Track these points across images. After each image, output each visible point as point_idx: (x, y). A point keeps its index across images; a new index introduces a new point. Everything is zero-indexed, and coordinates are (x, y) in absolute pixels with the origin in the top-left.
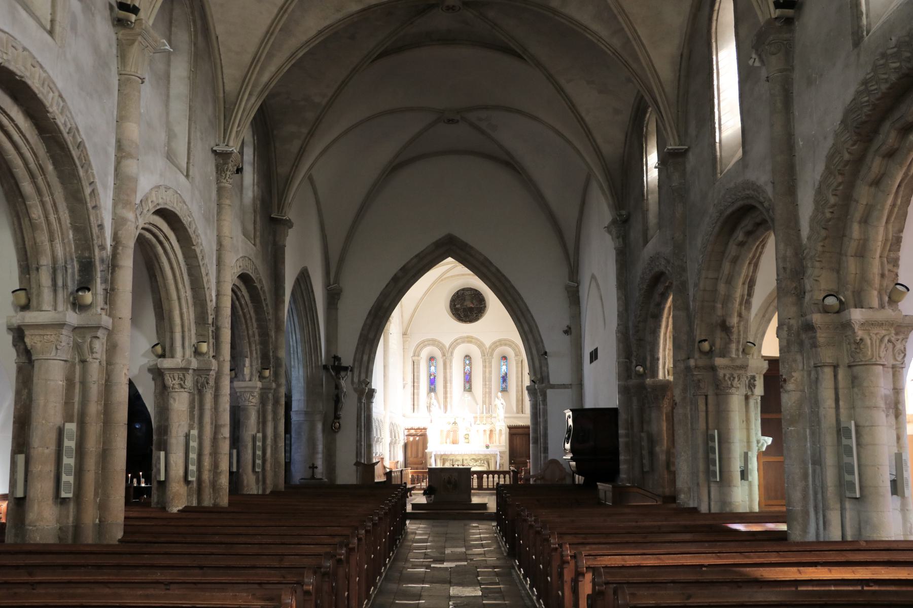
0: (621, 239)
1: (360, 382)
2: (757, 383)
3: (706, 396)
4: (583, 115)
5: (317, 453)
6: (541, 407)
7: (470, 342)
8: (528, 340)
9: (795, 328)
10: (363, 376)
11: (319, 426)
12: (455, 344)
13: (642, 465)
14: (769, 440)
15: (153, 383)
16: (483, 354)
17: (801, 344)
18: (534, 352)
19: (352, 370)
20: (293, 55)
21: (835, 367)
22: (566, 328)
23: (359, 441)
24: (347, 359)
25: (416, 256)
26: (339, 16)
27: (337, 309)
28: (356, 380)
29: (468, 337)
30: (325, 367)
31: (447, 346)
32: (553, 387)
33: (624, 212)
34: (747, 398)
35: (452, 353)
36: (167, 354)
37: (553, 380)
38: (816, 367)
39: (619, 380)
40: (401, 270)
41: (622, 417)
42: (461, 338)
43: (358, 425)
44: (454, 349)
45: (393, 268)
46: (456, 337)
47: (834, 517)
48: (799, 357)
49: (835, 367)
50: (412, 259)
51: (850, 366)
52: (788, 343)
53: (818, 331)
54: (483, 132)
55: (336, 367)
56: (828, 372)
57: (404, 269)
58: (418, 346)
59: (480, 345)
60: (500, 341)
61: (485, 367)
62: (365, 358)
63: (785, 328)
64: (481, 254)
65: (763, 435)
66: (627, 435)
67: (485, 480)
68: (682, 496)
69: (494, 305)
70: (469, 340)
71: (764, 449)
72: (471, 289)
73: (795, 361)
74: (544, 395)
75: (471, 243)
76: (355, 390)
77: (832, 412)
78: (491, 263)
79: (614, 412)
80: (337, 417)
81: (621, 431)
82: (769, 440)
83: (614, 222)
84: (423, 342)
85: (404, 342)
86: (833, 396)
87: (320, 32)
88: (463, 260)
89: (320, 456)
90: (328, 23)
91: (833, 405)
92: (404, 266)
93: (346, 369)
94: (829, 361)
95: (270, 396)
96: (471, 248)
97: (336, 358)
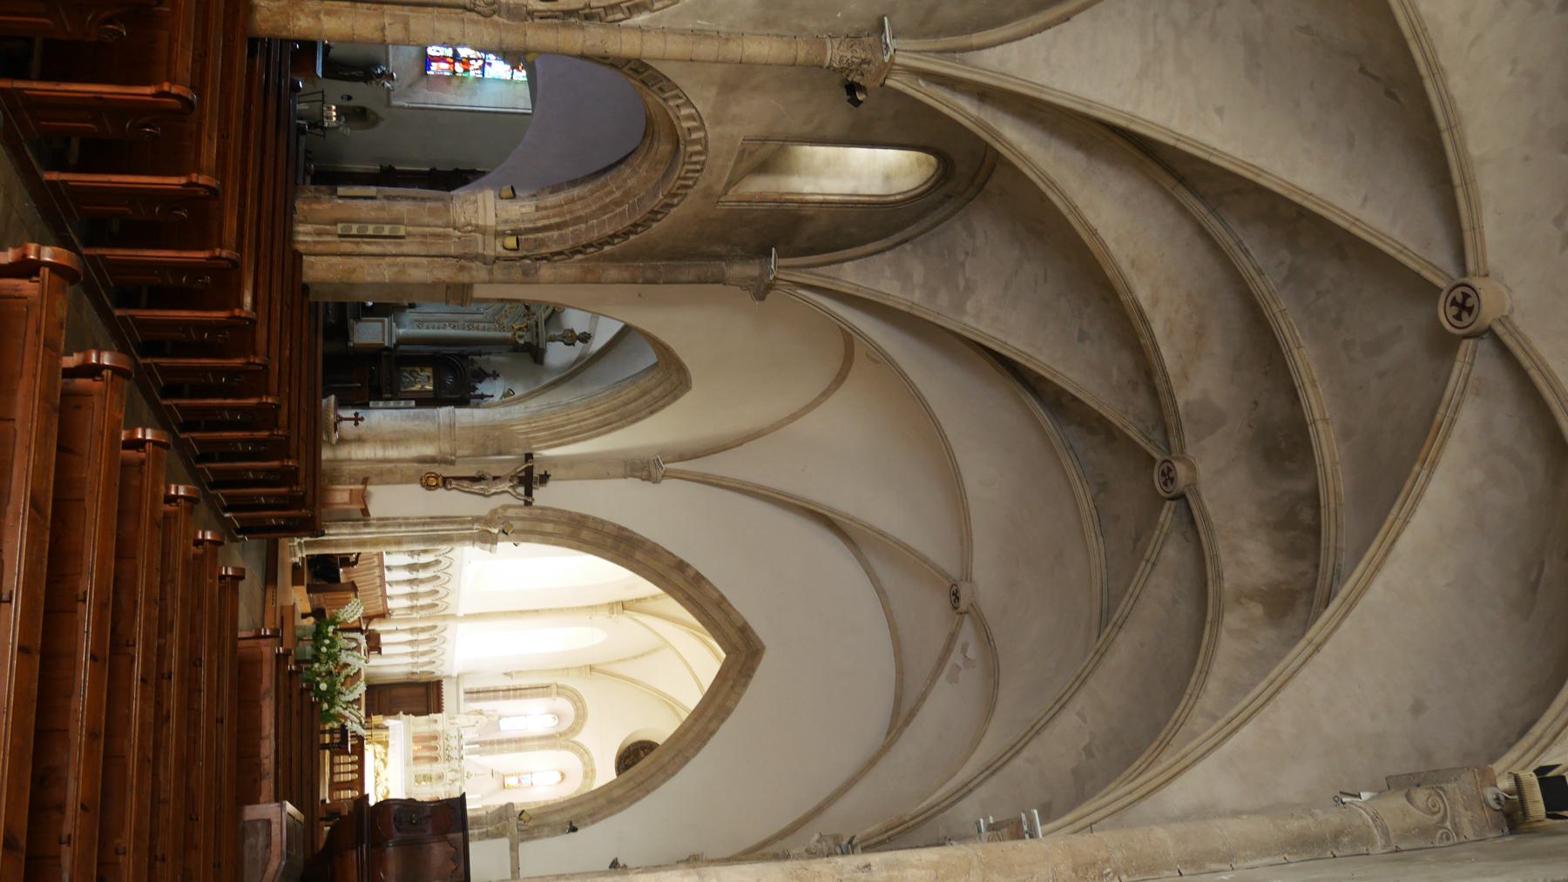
1: (506, 520)
4: (1025, 753)
5: (384, 448)
10: (517, 525)
11: (429, 450)
18: (577, 811)
19: (528, 504)
20: (1052, 184)
22: (621, 863)
23: (407, 522)
24: (541, 496)
26: (1125, 266)
27: (625, 477)
28: (510, 513)
29: (593, 771)
30: (529, 456)
31: (577, 739)
32: (514, 848)
35: (566, 747)
37: (526, 849)
40: (698, 573)
42: (591, 760)
43: (435, 520)
44: (573, 750)
45: (698, 561)
46: (593, 753)
50: (715, 589)
54: (943, 660)
55: (529, 479)
57: (699, 579)
58: (574, 692)
62: (549, 527)
64: (736, 703)
67: (343, 778)
74: (499, 835)
76: (494, 512)
84: (581, 700)
85: (579, 669)
87: (1094, 233)
88: (721, 676)
89: (380, 453)
90: (1112, 246)
92: (703, 578)
93: (529, 493)
96: (745, 685)
97: (544, 479)
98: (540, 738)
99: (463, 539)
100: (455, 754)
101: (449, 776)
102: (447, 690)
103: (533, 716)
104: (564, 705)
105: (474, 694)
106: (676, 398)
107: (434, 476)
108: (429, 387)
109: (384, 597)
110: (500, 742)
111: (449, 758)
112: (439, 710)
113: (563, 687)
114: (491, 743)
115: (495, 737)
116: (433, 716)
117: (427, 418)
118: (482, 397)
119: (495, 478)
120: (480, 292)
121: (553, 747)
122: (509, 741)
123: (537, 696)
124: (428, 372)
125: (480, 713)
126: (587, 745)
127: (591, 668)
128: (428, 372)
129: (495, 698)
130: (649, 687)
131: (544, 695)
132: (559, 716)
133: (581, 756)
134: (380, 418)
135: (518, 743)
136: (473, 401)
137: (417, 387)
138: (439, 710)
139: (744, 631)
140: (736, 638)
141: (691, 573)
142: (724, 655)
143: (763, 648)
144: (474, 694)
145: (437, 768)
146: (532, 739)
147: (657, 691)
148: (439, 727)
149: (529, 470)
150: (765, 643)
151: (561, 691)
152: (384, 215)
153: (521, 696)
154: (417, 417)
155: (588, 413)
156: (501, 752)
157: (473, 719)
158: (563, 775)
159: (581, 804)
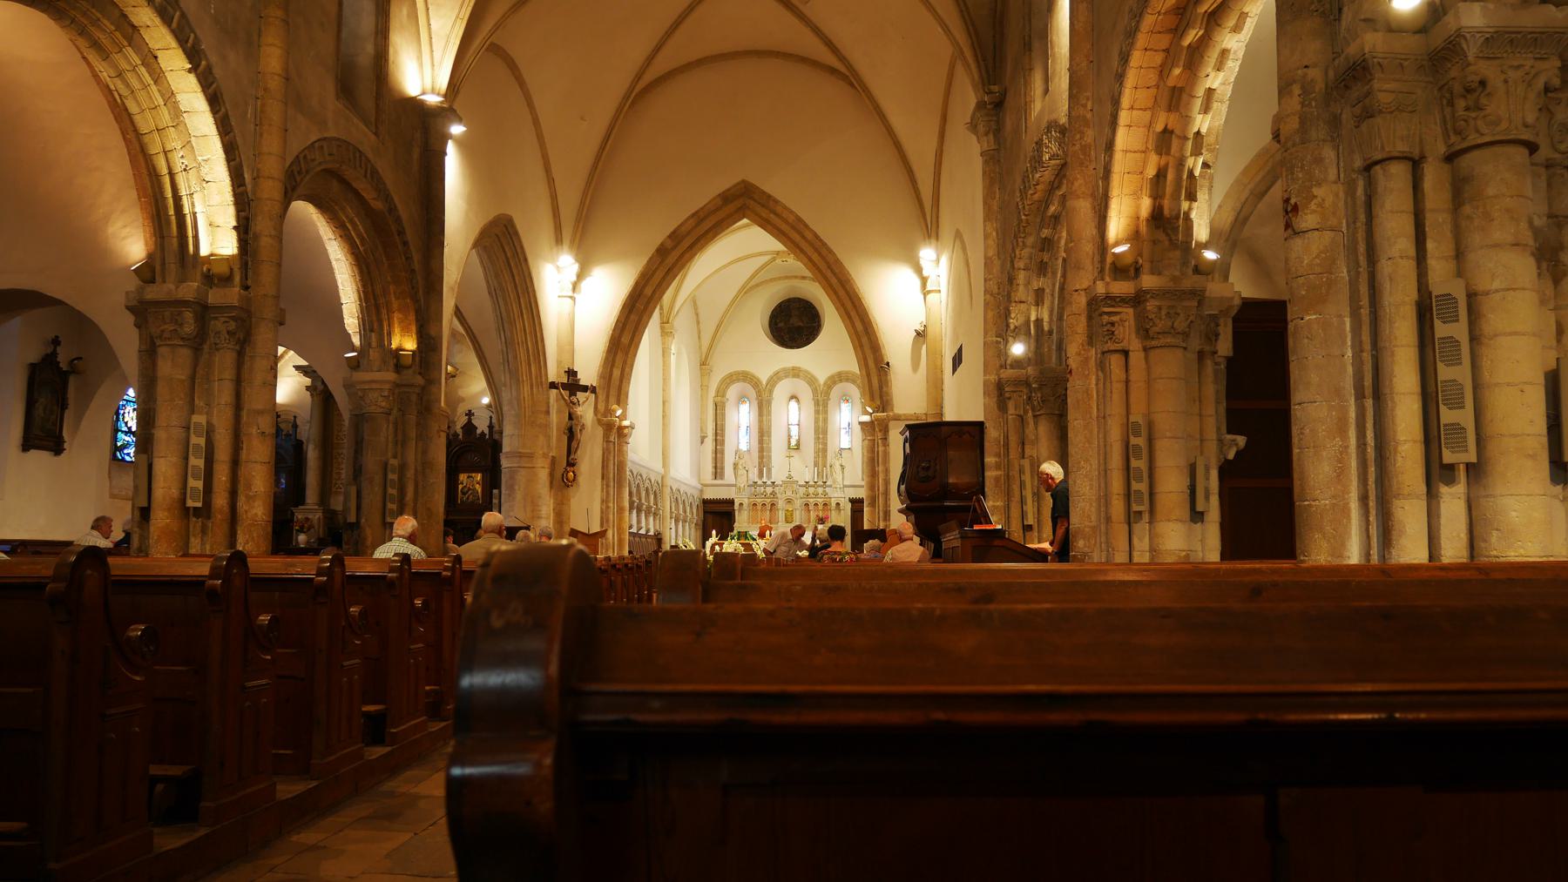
0: (991, 136)
2: (1221, 329)
3: (1126, 353)
6: (881, 449)
7: (796, 376)
8: (861, 346)
9: (1320, 86)
12: (776, 378)
13: (1023, 515)
14: (1241, 440)
15: (136, 331)
16: (815, 391)
17: (1335, 122)
21: (1416, 164)
24: (588, 376)
25: (693, 215)
33: (995, 88)
34: (1201, 355)
35: (771, 392)
36: (158, 278)
38: (1368, 168)
39: (986, 372)
41: (992, 434)
42: (784, 369)
46: (777, 368)
47: (1410, 516)
48: (1329, 153)
49: (1416, 164)
51: (1450, 158)
52: (1303, 122)
53: (1378, 75)
56: (1395, 180)
58: (723, 381)
59: (811, 381)
60: (839, 374)
61: (817, 412)
63: (1297, 90)
65: (1229, 432)
66: (998, 466)
68: (1081, 543)
69: (833, 325)
70: (795, 373)
71: (1231, 456)
72: (799, 300)
73: (1319, 160)
75: (767, 188)
77: (1408, 268)
78: (806, 226)
79: (979, 426)
80: (571, 464)
81: (990, 460)
82: (1241, 440)
83: (980, 105)
86: (1410, 228)
88: (765, 224)
91: (1412, 252)
93: (585, 389)
94: (1401, 147)
95: (414, 398)
97: (572, 373)
98: (760, 415)
99: (621, 452)
100: (769, 490)
101: (789, 493)
102: (710, 494)
103: (742, 418)
104: (733, 392)
105: (718, 472)
106: (516, 233)
107: (564, 477)
108: (479, 477)
109: (646, 536)
110: (761, 450)
111: (773, 493)
112: (731, 502)
113: (718, 391)
114: (761, 457)
115: (756, 455)
116: (736, 506)
117: (512, 478)
118: (491, 427)
119: (570, 418)
120: (1062, 113)
121: (769, 403)
122: (761, 442)
123: (723, 415)
124: (463, 477)
125: (735, 465)
126: (771, 373)
127: (703, 364)
128: (463, 477)
129: (723, 452)
130: (724, 316)
131: (723, 408)
132: (742, 398)
133: (780, 379)
134: (641, 451)
135: (763, 434)
136: (496, 437)
137: (479, 488)
138: (731, 502)
139: (726, 198)
140: (731, 207)
141: (669, 244)
142: (745, 221)
143: (743, 181)
144: (718, 472)
145: (781, 504)
146: (760, 422)
147: (731, 305)
148: (746, 502)
149: (564, 386)
150: (739, 179)
151: (721, 392)
152: (378, 479)
153: (723, 430)
154: (511, 488)
155: (519, 325)
156: (770, 450)
157: (741, 472)
158: (793, 397)
159: (865, 359)
